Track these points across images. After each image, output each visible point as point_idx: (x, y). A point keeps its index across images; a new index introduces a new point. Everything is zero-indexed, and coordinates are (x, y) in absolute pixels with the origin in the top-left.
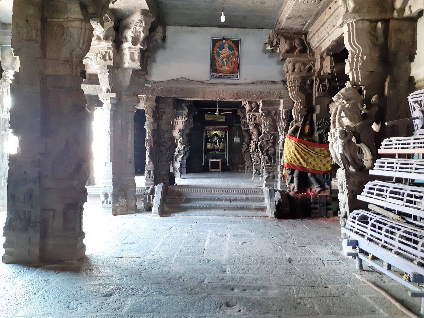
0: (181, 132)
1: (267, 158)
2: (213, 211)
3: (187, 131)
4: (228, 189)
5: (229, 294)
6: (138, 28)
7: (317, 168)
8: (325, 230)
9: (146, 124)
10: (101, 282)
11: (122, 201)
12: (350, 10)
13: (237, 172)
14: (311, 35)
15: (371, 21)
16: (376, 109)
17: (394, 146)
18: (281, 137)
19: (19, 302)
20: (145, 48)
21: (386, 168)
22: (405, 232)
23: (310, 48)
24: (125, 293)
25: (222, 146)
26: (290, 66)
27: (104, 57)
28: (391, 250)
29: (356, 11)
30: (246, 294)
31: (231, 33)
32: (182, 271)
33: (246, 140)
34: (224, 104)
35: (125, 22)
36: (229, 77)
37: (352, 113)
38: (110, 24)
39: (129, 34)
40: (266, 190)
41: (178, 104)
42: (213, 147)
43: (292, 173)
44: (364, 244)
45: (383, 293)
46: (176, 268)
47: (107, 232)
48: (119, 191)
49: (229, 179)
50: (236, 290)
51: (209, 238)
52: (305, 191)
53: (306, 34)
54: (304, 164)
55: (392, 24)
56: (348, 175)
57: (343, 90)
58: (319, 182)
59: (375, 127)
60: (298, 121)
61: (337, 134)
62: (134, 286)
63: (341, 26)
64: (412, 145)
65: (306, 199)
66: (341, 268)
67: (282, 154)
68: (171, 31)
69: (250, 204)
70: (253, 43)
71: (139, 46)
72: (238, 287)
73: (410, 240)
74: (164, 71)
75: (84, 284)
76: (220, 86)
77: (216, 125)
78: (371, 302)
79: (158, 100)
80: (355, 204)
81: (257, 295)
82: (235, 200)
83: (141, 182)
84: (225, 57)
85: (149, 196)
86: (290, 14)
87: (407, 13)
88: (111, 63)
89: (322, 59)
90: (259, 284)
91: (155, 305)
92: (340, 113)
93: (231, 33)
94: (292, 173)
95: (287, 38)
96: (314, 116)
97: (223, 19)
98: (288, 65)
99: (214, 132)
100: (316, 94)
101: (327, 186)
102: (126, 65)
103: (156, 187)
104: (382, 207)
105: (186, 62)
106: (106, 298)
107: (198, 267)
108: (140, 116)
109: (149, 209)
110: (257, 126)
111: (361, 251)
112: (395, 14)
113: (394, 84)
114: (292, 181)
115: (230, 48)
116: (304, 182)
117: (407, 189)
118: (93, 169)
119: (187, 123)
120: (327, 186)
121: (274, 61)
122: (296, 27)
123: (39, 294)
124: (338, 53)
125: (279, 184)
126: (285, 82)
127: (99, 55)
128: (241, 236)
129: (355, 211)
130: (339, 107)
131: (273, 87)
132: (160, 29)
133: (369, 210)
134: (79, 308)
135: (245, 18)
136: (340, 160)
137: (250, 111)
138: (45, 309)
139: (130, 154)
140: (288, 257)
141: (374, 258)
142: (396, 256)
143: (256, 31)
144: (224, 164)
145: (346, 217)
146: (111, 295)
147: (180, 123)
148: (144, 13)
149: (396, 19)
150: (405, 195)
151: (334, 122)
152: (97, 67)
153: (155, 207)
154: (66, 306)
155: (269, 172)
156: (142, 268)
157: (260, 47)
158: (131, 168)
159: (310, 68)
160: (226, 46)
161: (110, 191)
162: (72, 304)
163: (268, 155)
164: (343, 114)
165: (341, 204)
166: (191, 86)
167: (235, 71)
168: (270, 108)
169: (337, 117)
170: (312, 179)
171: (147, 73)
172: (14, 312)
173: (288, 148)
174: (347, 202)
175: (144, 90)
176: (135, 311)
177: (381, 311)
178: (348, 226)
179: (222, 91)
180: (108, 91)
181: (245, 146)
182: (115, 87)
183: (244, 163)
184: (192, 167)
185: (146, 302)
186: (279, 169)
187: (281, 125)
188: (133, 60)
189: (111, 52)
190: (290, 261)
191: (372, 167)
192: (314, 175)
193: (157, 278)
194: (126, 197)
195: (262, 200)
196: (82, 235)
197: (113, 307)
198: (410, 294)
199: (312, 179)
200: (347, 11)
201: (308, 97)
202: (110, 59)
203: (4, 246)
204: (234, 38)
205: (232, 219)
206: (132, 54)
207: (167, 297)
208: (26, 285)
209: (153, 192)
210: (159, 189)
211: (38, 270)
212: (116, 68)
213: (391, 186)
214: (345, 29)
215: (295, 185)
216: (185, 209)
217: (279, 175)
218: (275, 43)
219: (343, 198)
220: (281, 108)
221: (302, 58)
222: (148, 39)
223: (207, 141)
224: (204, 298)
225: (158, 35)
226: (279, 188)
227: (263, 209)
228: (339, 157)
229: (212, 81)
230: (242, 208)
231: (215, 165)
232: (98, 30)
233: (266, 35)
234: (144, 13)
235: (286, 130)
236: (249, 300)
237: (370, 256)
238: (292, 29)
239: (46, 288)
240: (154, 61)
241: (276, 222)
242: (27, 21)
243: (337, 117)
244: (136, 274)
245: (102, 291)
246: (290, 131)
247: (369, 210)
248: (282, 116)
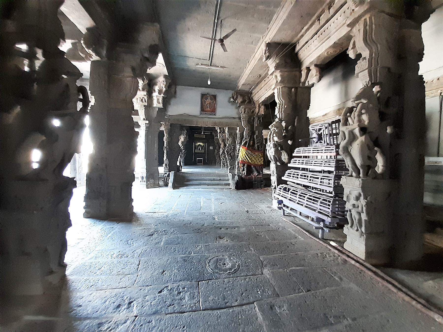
0: (182, 142)
1: (230, 158)
2: (201, 186)
3: (185, 143)
4: (209, 174)
5: (219, 231)
6: (162, 85)
7: (256, 163)
8: (262, 195)
9: (165, 138)
10: (145, 228)
11: (152, 181)
12: (279, 81)
13: (212, 165)
14: (254, 95)
15: (289, 88)
16: (291, 133)
17: (302, 152)
18: (238, 147)
19: (96, 241)
20: (166, 96)
21: (297, 163)
22: (310, 196)
23: (253, 102)
24: (161, 234)
25: (203, 151)
26: (243, 110)
27: (142, 100)
28: (302, 205)
29: (281, 82)
30: (228, 231)
31: (212, 91)
32: (191, 219)
33: (217, 148)
34: (206, 129)
35: (154, 81)
36: (210, 114)
37: (279, 135)
38: (146, 82)
39: (157, 88)
40: (230, 175)
41: (182, 127)
42: (199, 151)
43: (244, 166)
44: (286, 202)
45: (299, 227)
46: (188, 218)
47: (147, 199)
48: (149, 175)
49: (208, 169)
50: (222, 229)
51: (202, 200)
52: (250, 175)
53: (251, 93)
54: (250, 161)
55: (299, 89)
56: (277, 167)
57: (274, 123)
58: (257, 171)
59: (290, 142)
60: (246, 138)
61: (272, 145)
62: (165, 229)
63: (274, 89)
64: (312, 152)
65: (251, 179)
66: (274, 215)
67: (238, 155)
68: (179, 88)
69: (221, 182)
70: (223, 98)
71: (162, 95)
72: (223, 227)
73: (315, 200)
74: (175, 110)
75: (135, 229)
76: (205, 119)
77: (200, 140)
78: (294, 233)
79: (171, 125)
80: (280, 181)
81: (235, 231)
82: (214, 180)
83: (162, 170)
84: (208, 104)
85: (167, 179)
86: (244, 83)
87: (307, 84)
88: (146, 104)
89: (259, 107)
90: (234, 225)
91: (179, 240)
92: (273, 135)
93: (212, 91)
94: (244, 166)
95: (241, 95)
96: (255, 136)
97: (209, 83)
98: (242, 109)
99: (199, 143)
100: (256, 125)
101: (261, 172)
102: (155, 106)
103: (170, 173)
104: (295, 183)
105: (187, 105)
106: (150, 237)
107: (200, 217)
108: (161, 134)
109: (166, 185)
110: (223, 141)
111: (284, 206)
112: (301, 85)
113: (299, 121)
114: (244, 170)
115: (211, 99)
116: (250, 171)
117: (310, 174)
118: (358, 149)
119: (185, 138)
120: (261, 172)
121: (234, 107)
122: (246, 90)
123: (108, 236)
124: (270, 104)
125: (236, 171)
126: (240, 118)
127: (139, 99)
128: (219, 199)
129: (281, 185)
130: (273, 132)
131: (234, 120)
132: (173, 87)
133: (288, 185)
134: (134, 244)
135: (219, 83)
136: (273, 159)
137: (220, 132)
138: (113, 245)
139: (156, 155)
140: (246, 210)
141: (292, 209)
142: (306, 208)
143: (225, 91)
144: (204, 160)
145: (275, 188)
146: (153, 235)
147: (182, 139)
148: (165, 76)
149: (301, 87)
150: (309, 177)
151: (270, 139)
152: (138, 106)
153: (170, 184)
154: (126, 242)
155: (231, 165)
156: (168, 218)
157: (227, 99)
158: (157, 162)
159: (253, 112)
160: (209, 98)
161: (145, 175)
162: (129, 241)
163: (230, 156)
164: (274, 135)
165: (272, 182)
166: (190, 118)
167: (213, 111)
168: (232, 131)
169: (272, 136)
170: (254, 169)
171: (166, 111)
172: (94, 248)
173: (242, 153)
174: (276, 181)
175: (165, 120)
176: (169, 244)
177: (299, 237)
178: (277, 193)
179: (206, 122)
180: (144, 119)
181: (216, 151)
182: (148, 117)
183: (218, 160)
184: (188, 162)
185: (174, 238)
186: (236, 164)
187: (238, 141)
188: (159, 103)
189: (146, 98)
190: (247, 212)
191: (289, 162)
192: (255, 166)
193: (178, 224)
194: (153, 178)
195: (228, 180)
196: (132, 200)
197: (155, 242)
198: (314, 228)
199: (254, 169)
200: (277, 82)
201: (252, 126)
202: (145, 101)
203: (84, 208)
204: (213, 94)
205: (213, 190)
206: (158, 99)
207: (186, 235)
208: (100, 231)
209: (169, 176)
210: (172, 174)
211: (106, 222)
212: (148, 107)
213: (300, 172)
214: (276, 91)
215: (245, 171)
216: (187, 185)
217: (236, 167)
218: (235, 98)
219: (274, 179)
220: (238, 131)
221: (249, 106)
222: (166, 93)
223: (195, 148)
224: (206, 234)
225: (173, 90)
226: (236, 173)
227: (229, 184)
228: (272, 158)
229: (201, 116)
230: (218, 185)
231: (200, 161)
232: (141, 83)
233: (230, 93)
234: (165, 76)
235: (241, 143)
236: (231, 235)
237: (289, 208)
238: (244, 90)
239: (112, 232)
240: (170, 104)
241: (236, 191)
242: (99, 75)
243: (272, 136)
244: (165, 222)
245: (147, 234)
246: (243, 144)
247: (288, 185)
248: (238, 136)
